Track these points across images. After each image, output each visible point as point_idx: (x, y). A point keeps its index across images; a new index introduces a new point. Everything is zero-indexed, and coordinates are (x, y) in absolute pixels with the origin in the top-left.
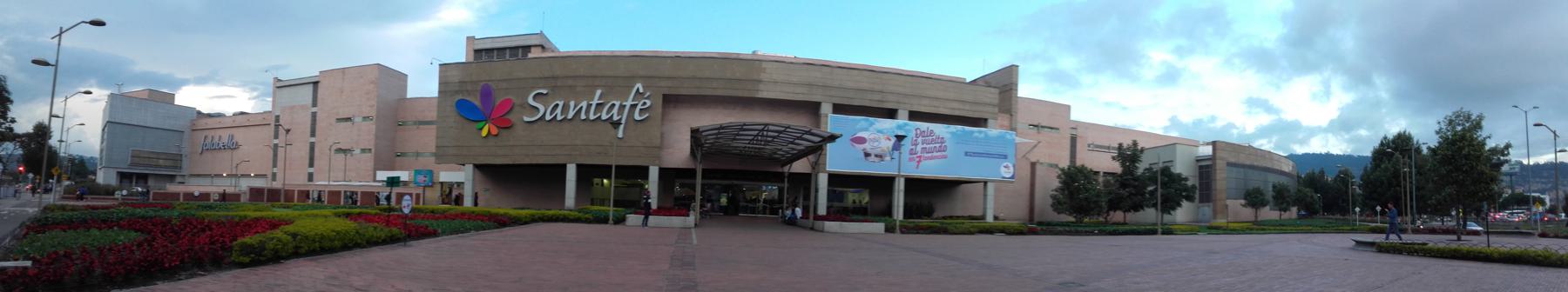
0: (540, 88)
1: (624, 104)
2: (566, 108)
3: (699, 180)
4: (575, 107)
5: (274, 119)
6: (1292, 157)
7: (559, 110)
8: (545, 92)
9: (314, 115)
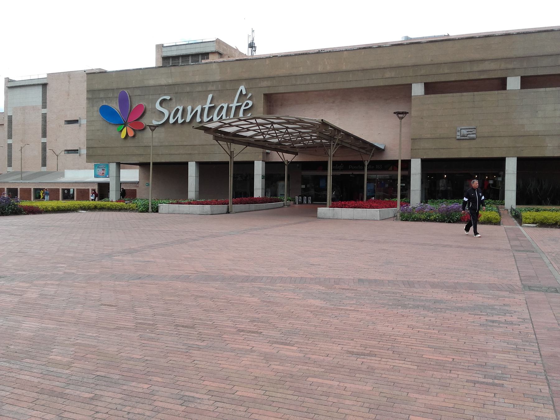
0: (165, 95)
1: (230, 106)
2: (184, 111)
3: (330, 172)
4: (192, 110)
5: (6, 119)
7: (179, 115)
9: (44, 117)
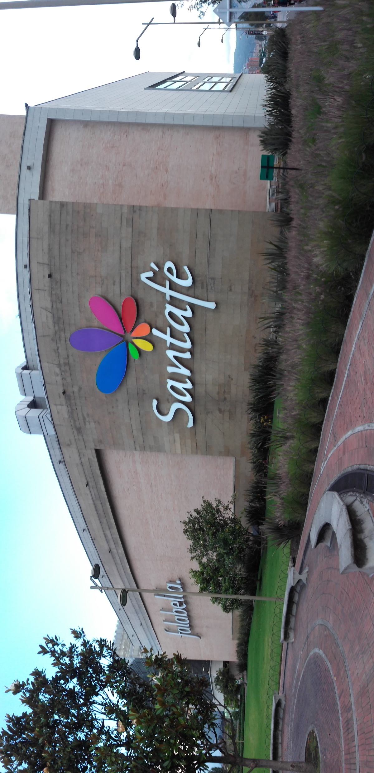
1: (168, 298)
6: (296, 557)
7: (179, 386)
8: (155, 403)
